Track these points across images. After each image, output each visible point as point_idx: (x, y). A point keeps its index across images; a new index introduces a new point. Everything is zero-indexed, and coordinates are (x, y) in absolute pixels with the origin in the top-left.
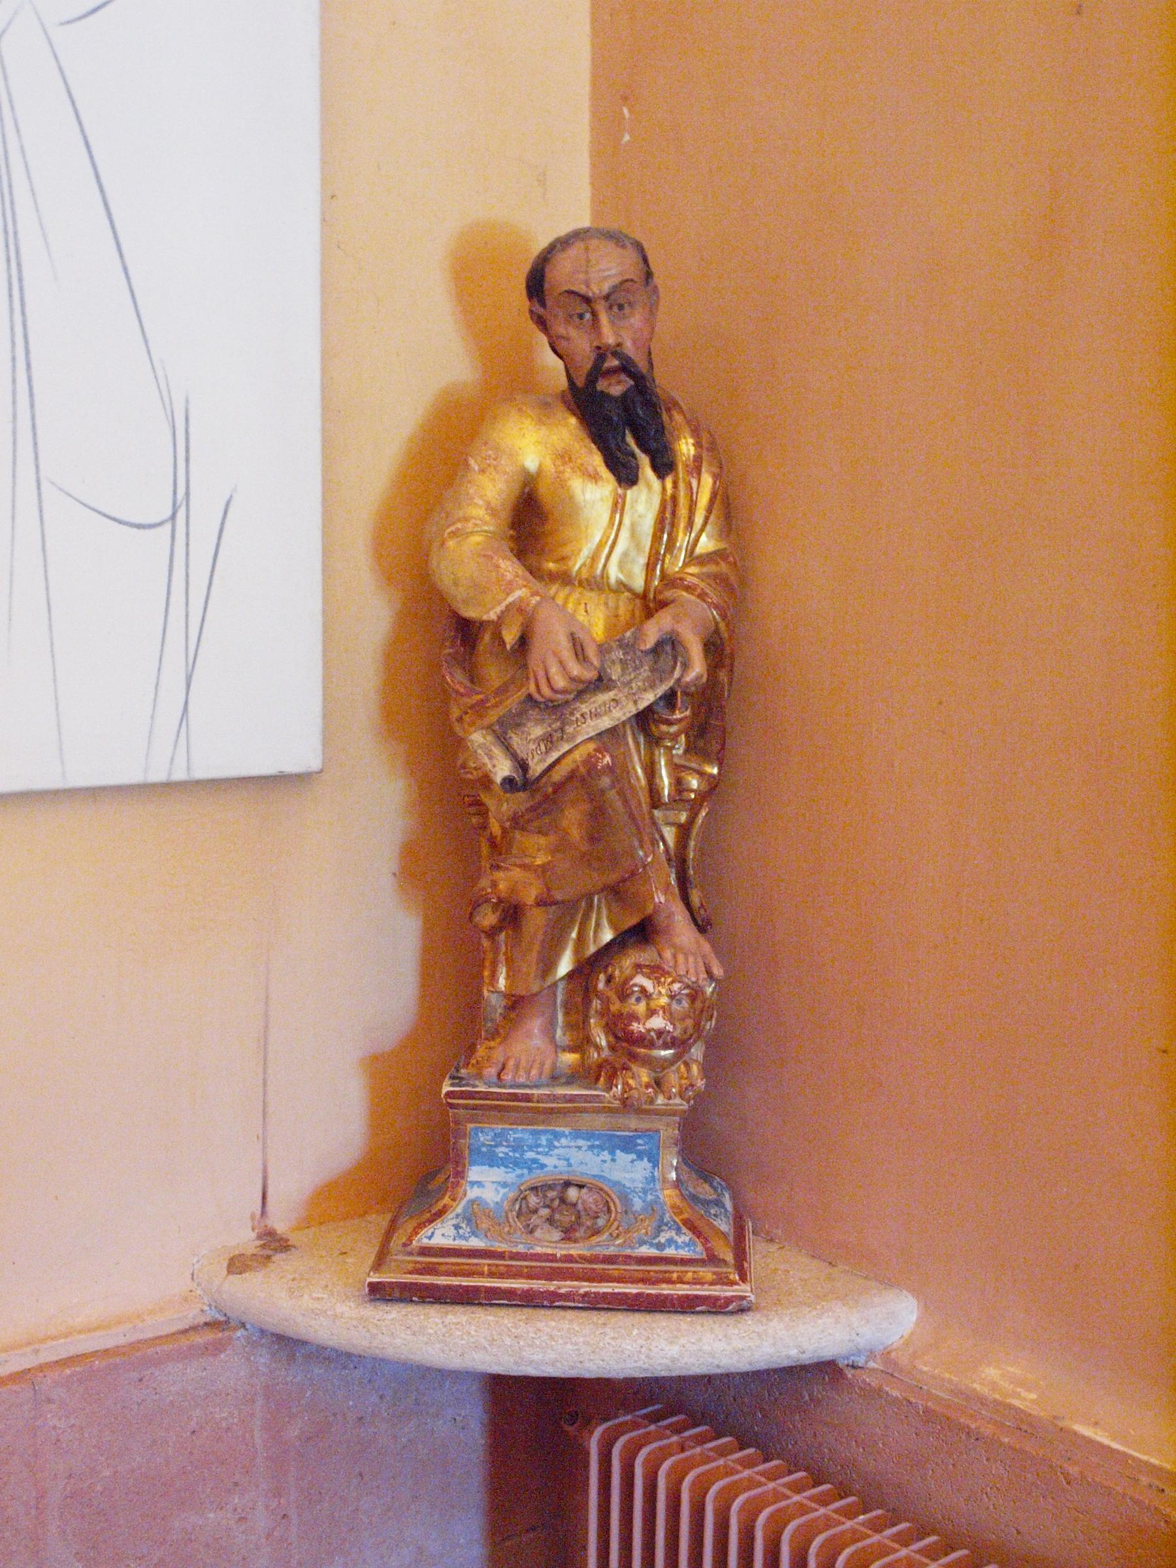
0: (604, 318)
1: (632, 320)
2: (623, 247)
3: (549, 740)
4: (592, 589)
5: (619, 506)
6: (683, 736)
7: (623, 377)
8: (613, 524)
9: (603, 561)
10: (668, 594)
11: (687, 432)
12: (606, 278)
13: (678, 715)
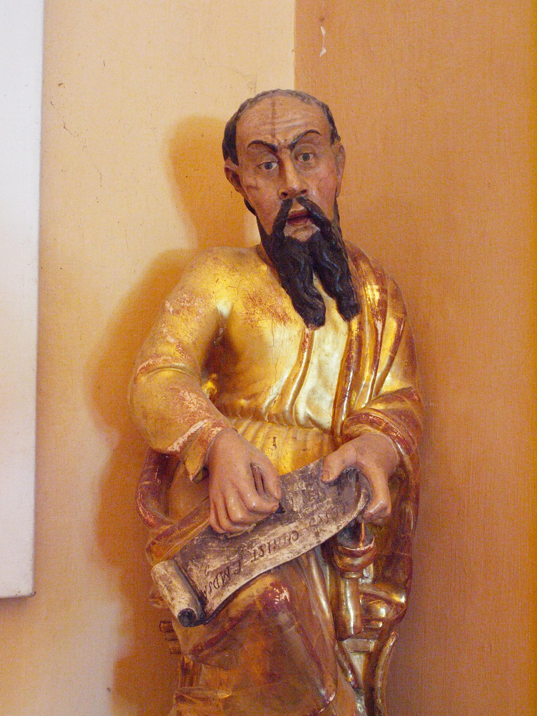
0: (289, 166)
1: (317, 170)
2: (309, 103)
3: (226, 574)
4: (282, 425)
5: (307, 345)
6: (371, 566)
7: (309, 223)
8: (304, 364)
9: (291, 397)
10: (354, 429)
11: (371, 278)
12: (294, 127)
13: (362, 548)
